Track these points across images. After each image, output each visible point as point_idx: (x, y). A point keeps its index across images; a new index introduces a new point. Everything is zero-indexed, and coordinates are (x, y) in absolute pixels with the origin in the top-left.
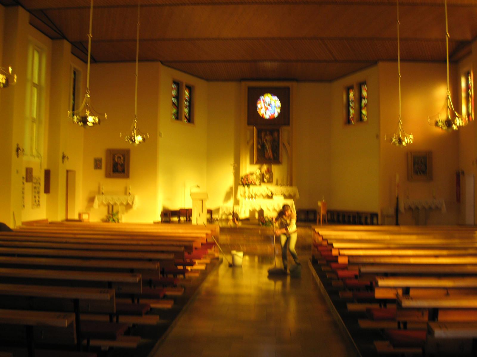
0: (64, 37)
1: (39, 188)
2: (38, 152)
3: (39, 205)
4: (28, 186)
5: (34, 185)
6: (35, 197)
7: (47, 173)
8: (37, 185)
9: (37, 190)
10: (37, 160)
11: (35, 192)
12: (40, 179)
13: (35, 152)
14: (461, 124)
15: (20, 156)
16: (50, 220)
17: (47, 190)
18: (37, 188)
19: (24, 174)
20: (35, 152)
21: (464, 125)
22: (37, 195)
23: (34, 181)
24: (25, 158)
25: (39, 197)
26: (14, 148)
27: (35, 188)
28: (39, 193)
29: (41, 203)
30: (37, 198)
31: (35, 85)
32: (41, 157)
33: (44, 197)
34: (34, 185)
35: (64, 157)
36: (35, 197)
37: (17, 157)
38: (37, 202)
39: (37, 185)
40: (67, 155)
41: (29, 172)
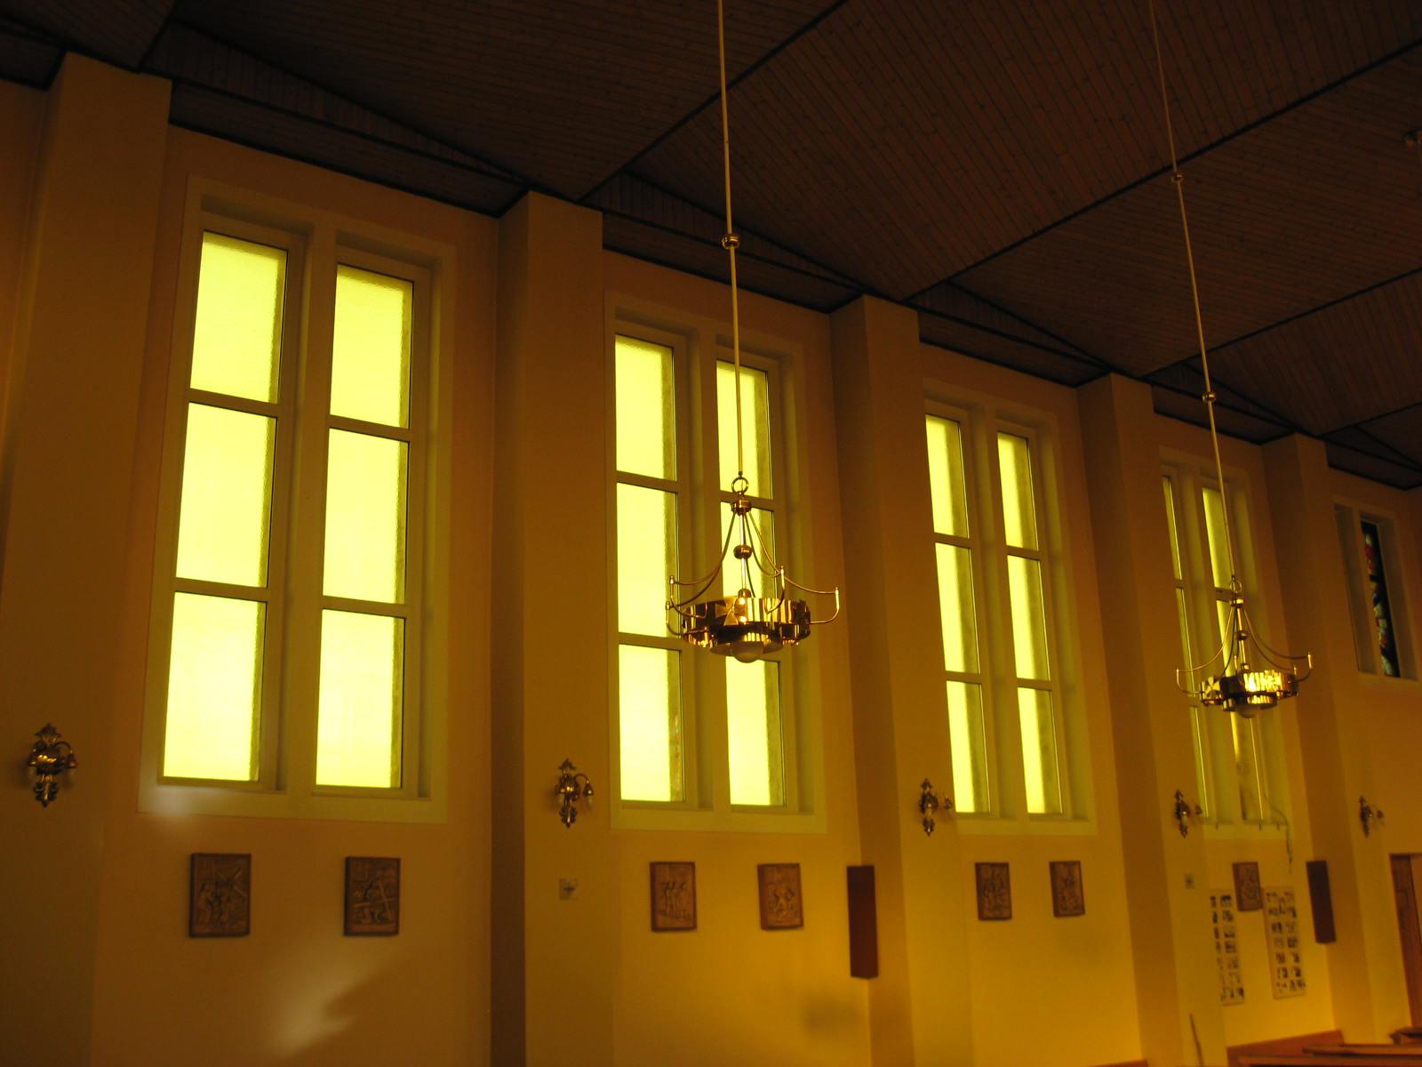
0: (1293, 428)
1: (1292, 927)
2: (1273, 808)
3: (1301, 984)
4: (1250, 927)
5: (1273, 919)
6: (1281, 958)
7: (1318, 874)
8: (1285, 919)
9: (1286, 935)
10: (1272, 834)
11: (1278, 942)
12: (1290, 895)
13: (1263, 810)
14: (753, 634)
15: (1371, 831)
16: (1351, 1039)
17: (1325, 932)
18: (1285, 929)
19: (1227, 884)
20: (1263, 810)
21: (749, 634)
22: (1287, 951)
23: (1271, 904)
24: (1208, 831)
25: (1297, 959)
26: (1167, 806)
27: (1277, 927)
28: (1292, 943)
29: (1308, 976)
30: (1290, 961)
31: (1222, 594)
32: (1287, 824)
33: (1315, 958)
34: (1273, 919)
35: (1364, 814)
36: (1281, 958)
37: (1182, 837)
38: (1292, 976)
39: (1285, 919)
40: (1376, 803)
41: (1246, 877)
